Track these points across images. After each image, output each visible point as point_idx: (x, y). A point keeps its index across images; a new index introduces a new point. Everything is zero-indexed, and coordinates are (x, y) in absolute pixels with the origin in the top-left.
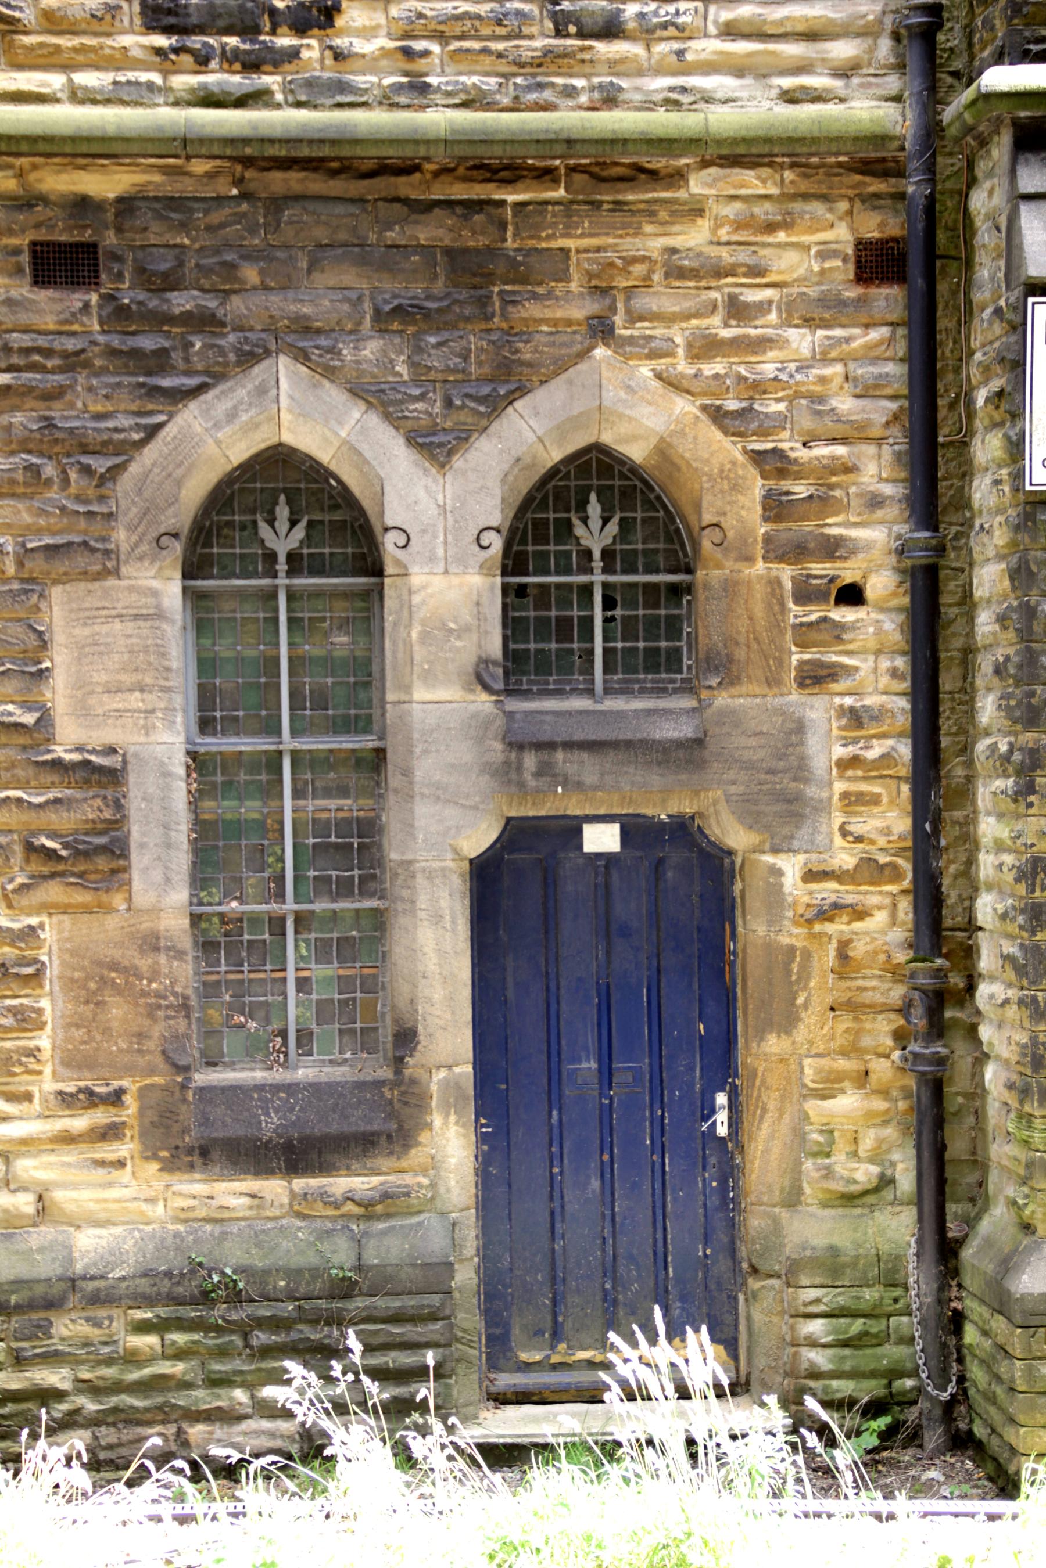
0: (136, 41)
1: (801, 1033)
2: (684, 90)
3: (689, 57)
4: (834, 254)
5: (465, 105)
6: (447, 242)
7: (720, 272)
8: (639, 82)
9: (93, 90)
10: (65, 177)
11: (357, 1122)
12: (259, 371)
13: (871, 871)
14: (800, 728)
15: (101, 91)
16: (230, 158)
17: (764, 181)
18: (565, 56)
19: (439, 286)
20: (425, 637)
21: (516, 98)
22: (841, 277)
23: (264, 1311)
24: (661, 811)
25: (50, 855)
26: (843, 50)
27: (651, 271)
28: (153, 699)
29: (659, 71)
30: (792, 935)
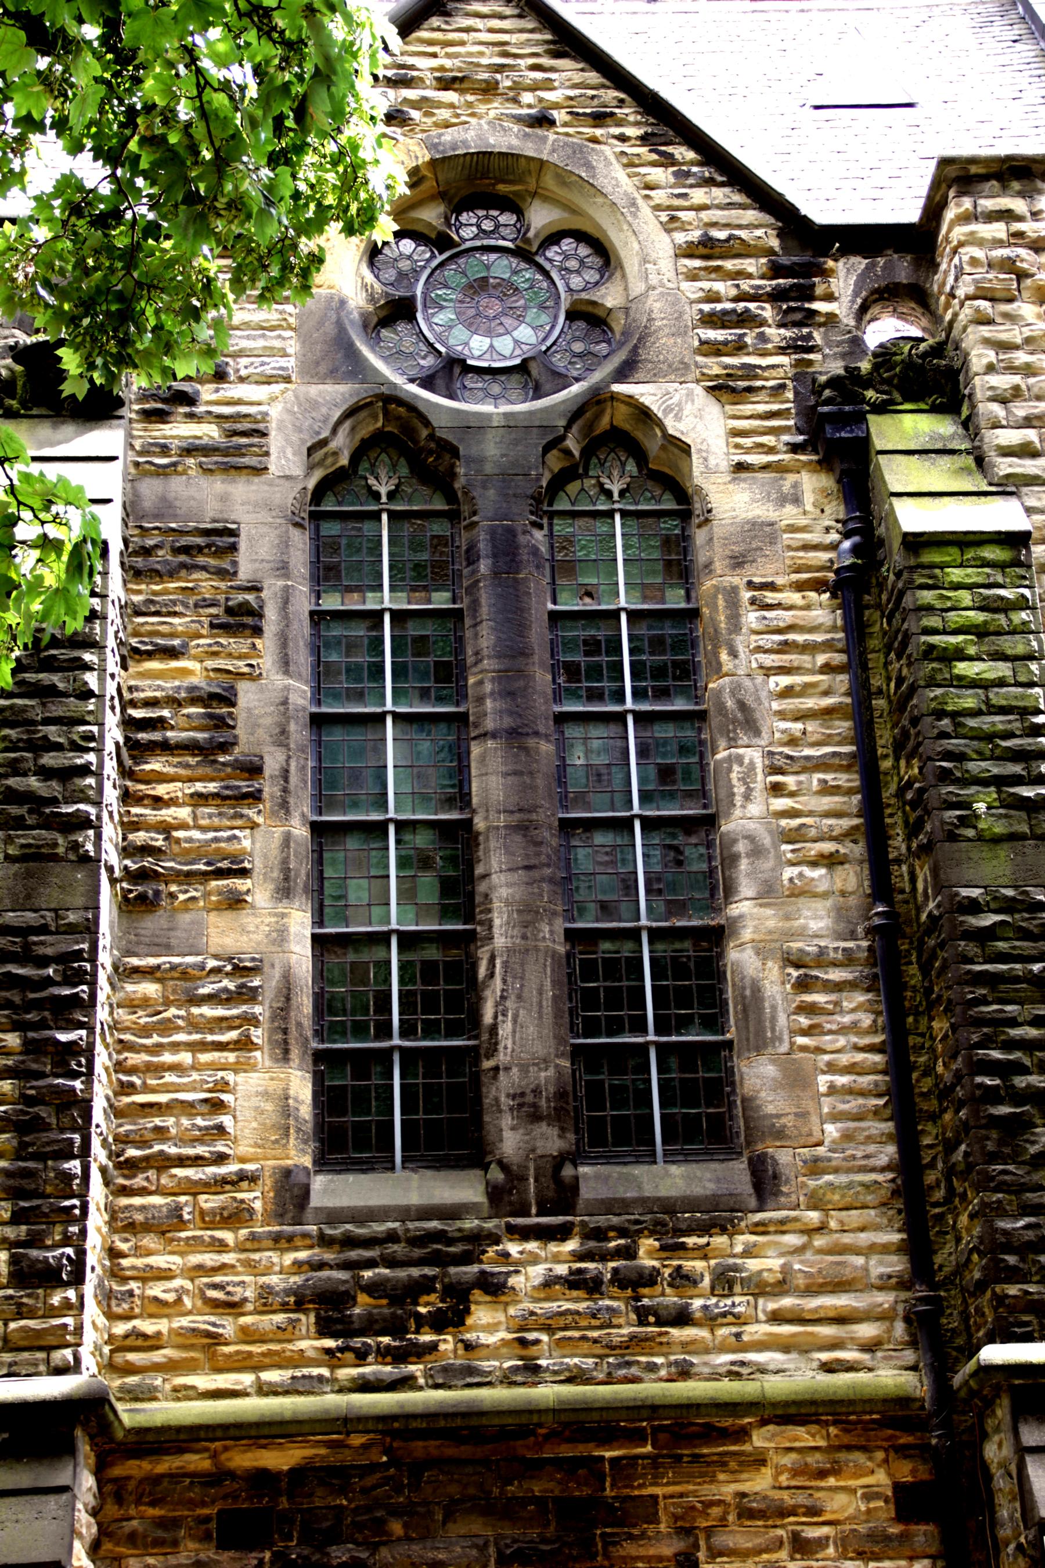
2: (743, 1364)
3: (745, 1338)
4: (877, 1496)
5: (569, 1380)
6: (557, 1493)
7: (783, 1512)
8: (706, 1358)
9: (276, 1384)
10: (249, 1455)
15: (282, 1385)
16: (381, 1432)
17: (813, 1436)
18: (647, 1340)
21: (609, 1374)
22: (884, 1516)
26: (867, 1331)
27: (726, 1513)
29: (722, 1349)
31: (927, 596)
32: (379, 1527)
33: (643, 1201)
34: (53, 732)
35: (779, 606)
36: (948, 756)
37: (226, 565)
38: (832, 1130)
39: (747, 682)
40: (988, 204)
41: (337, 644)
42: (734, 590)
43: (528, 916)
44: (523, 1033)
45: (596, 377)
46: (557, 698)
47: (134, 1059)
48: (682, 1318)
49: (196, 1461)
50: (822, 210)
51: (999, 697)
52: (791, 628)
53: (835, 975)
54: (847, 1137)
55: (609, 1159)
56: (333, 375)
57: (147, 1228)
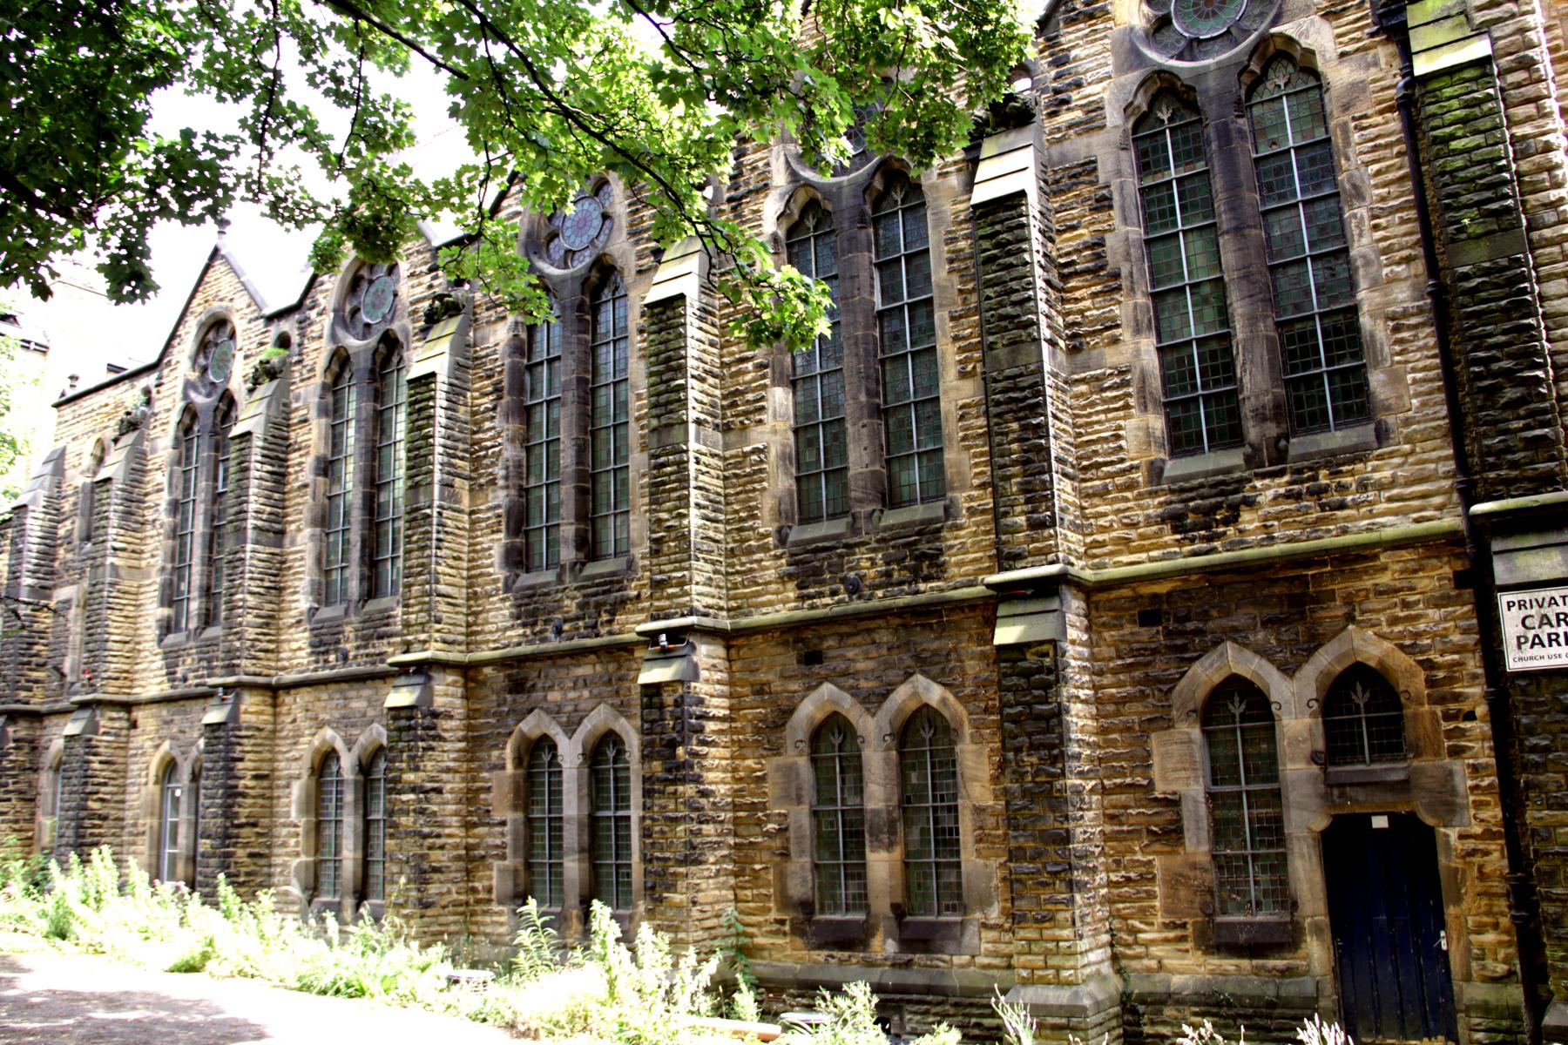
0: (1169, 538)
1: (1464, 906)
7: (1396, 591)
11: (1276, 939)
13: (1488, 835)
14: (1451, 774)
19: (1285, 609)
20: (1290, 744)
23: (1242, 1012)
24: (1403, 809)
25: (1155, 833)
26: (1437, 500)
29: (1363, 518)
30: (1457, 863)
31: (1432, 109)
32: (1206, 613)
33: (1319, 453)
34: (1014, 285)
35: (1370, 126)
36: (1448, 196)
37: (1092, 178)
39: (1356, 173)
41: (1154, 205)
42: (1346, 124)
43: (1252, 320)
44: (1255, 380)
46: (1264, 204)
47: (1080, 421)
48: (1342, 506)
49: (1126, 592)
51: (1476, 156)
52: (1378, 137)
53: (1413, 321)
54: (1424, 404)
55: (1308, 432)
56: (1131, 68)
57: (1094, 495)
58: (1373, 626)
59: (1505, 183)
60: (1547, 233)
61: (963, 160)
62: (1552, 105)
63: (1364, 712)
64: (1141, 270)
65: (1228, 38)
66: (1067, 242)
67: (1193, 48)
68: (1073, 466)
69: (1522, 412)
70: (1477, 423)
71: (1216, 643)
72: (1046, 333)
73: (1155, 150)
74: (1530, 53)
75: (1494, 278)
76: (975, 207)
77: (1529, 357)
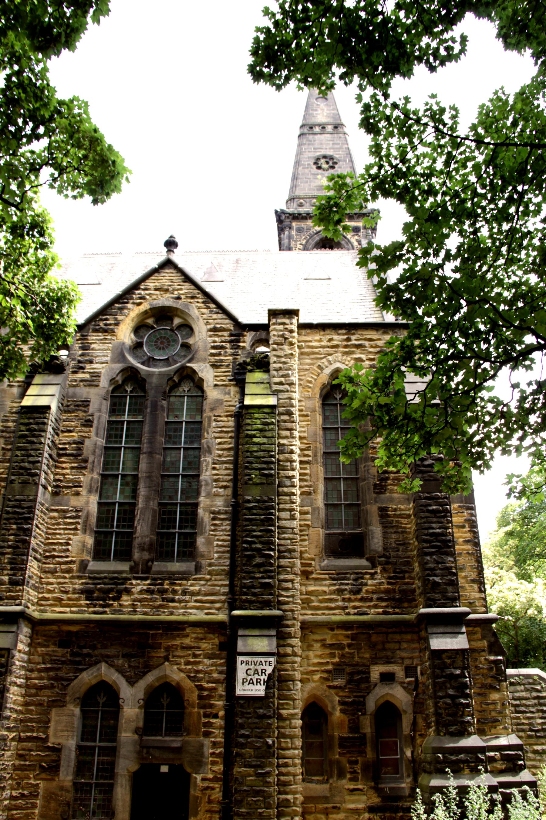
0: (83, 602)
12: (98, 665)
13: (215, 780)
14: (202, 745)
24: (177, 763)
26: (218, 605)
28: (70, 733)
29: (182, 608)
30: (198, 794)
31: (248, 421)
34: (32, 452)
36: (248, 462)
38: (216, 555)
40: (279, 321)
41: (113, 430)
43: (148, 499)
44: (143, 529)
45: (184, 361)
46: (165, 444)
48: (173, 601)
49: (55, 627)
50: (244, 319)
51: (263, 447)
53: (222, 516)
54: (220, 558)
55: (163, 560)
56: (119, 362)
58: (177, 664)
59: (272, 463)
60: (286, 490)
61: (23, 382)
62: (296, 434)
63: (166, 707)
64: (99, 461)
65: (167, 362)
66: (65, 438)
67: (150, 361)
68: (41, 555)
69: (262, 570)
70: (242, 571)
71: (97, 663)
72: (43, 481)
73: (120, 404)
74: (292, 409)
75: (260, 505)
76: (23, 407)
77: (269, 544)
